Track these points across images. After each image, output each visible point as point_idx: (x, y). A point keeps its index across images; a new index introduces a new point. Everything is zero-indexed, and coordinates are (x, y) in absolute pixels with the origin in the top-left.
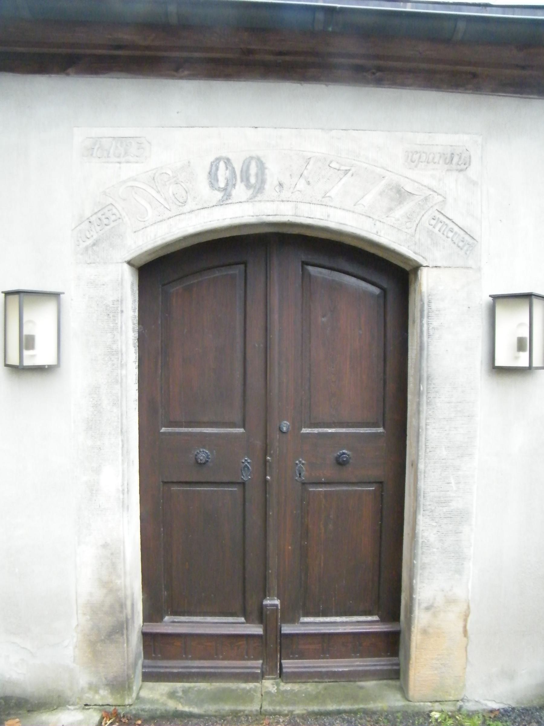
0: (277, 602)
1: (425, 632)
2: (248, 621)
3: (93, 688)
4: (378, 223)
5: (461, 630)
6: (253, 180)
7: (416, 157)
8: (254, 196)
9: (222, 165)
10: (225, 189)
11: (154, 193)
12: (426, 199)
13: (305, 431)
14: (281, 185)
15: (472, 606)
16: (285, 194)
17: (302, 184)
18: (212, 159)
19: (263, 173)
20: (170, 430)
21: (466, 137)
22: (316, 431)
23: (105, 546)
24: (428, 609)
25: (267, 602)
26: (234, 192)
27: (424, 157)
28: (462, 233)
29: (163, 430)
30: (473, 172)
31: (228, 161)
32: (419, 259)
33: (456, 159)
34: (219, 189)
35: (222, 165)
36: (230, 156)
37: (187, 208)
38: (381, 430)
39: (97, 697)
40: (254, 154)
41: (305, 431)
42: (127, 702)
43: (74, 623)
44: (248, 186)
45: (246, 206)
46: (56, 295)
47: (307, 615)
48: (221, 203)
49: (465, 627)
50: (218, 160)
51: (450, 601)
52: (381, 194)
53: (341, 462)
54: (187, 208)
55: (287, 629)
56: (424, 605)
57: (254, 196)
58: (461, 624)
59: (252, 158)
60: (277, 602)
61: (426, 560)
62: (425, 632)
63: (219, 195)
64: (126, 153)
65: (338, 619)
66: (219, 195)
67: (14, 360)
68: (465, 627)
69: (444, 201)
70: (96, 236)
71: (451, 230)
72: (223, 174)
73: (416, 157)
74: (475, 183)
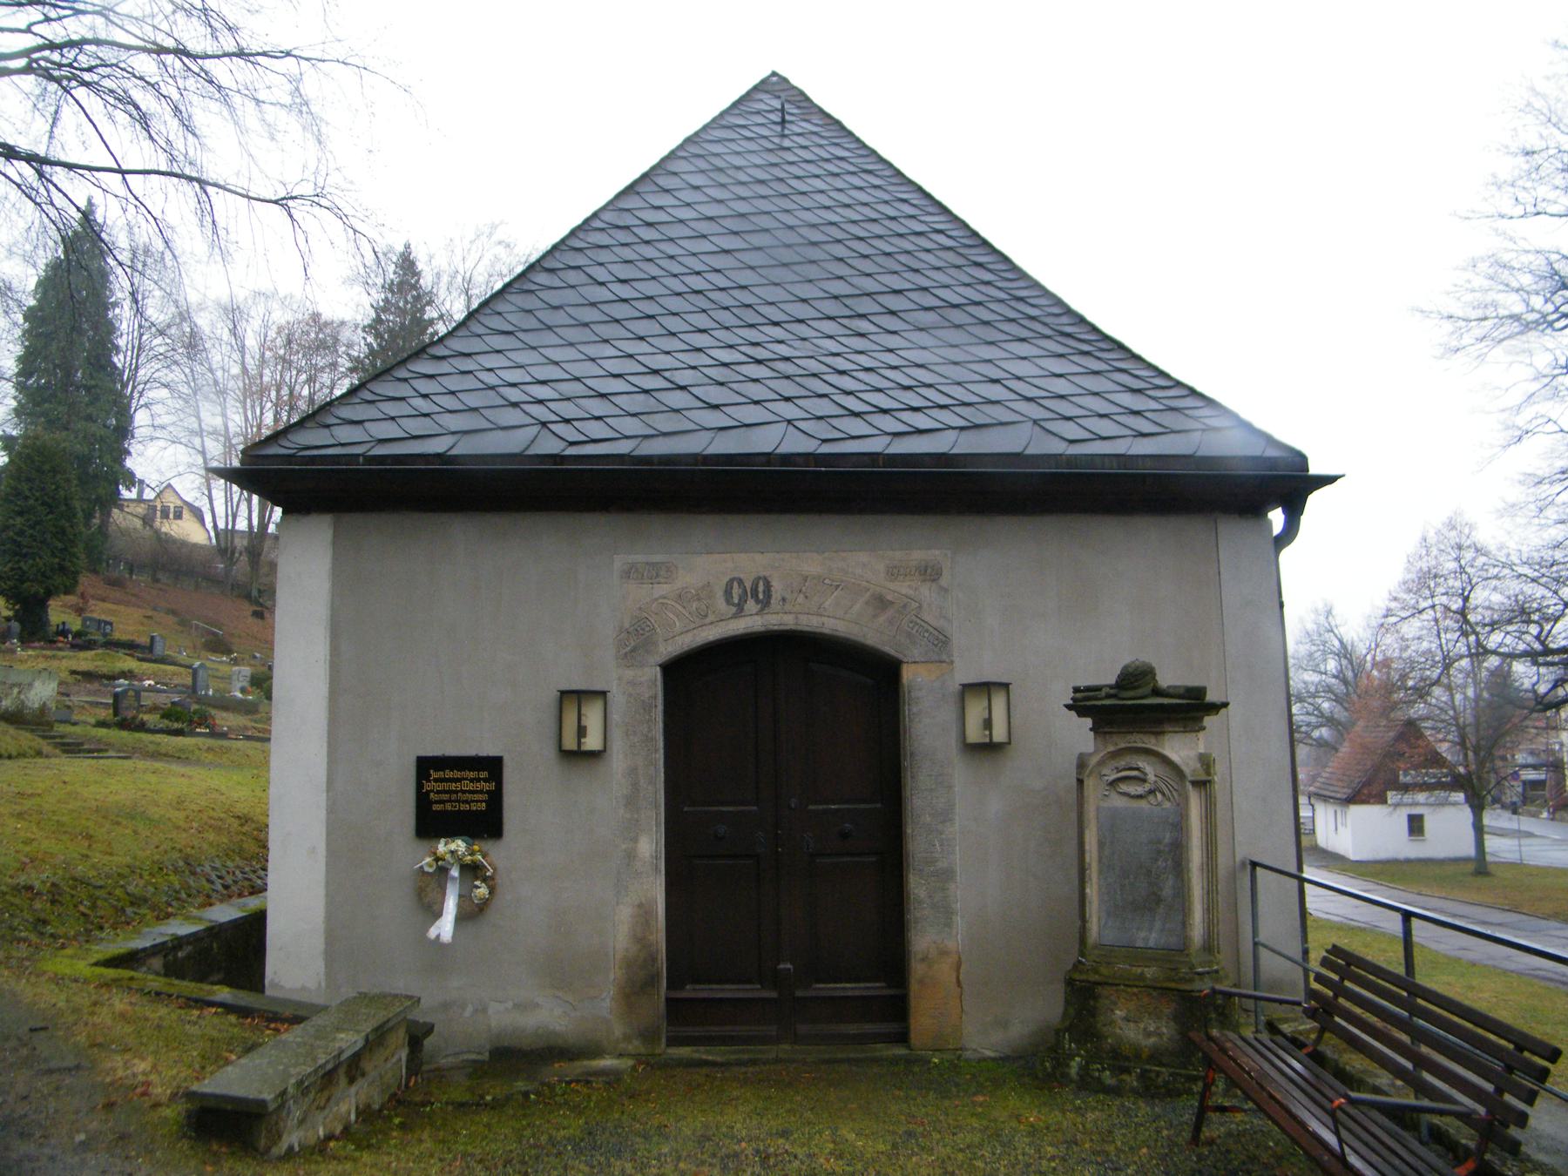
0: (789, 966)
1: (921, 982)
2: (763, 987)
3: (627, 1038)
4: (1474, 582)
5: (954, 980)
6: (761, 596)
7: (895, 571)
8: (762, 609)
9: (735, 584)
10: (739, 604)
11: (680, 608)
12: (905, 606)
13: (811, 807)
14: (784, 600)
15: (963, 958)
16: (788, 607)
17: (801, 599)
18: (727, 579)
19: (769, 590)
20: (691, 809)
21: (937, 552)
22: (821, 807)
23: (640, 906)
24: (923, 960)
25: (781, 966)
26: (746, 607)
27: (902, 571)
28: (936, 633)
29: (686, 809)
30: (944, 581)
31: (740, 582)
32: (900, 656)
33: (929, 571)
34: (733, 605)
35: (735, 584)
36: (742, 576)
37: (708, 620)
38: (879, 805)
39: (630, 1047)
40: (761, 574)
41: (811, 807)
42: (657, 1052)
43: (612, 977)
44: (758, 601)
45: (756, 617)
46: (603, 694)
47: (818, 981)
48: (735, 616)
49: (958, 978)
50: (732, 580)
51: (944, 953)
52: (867, 603)
53: (844, 836)
54: (708, 620)
55: (799, 993)
56: (920, 956)
57: (762, 609)
58: (954, 976)
59: (759, 578)
60: (789, 966)
61: (918, 915)
62: (921, 982)
63: (734, 609)
64: (657, 576)
65: (848, 985)
66: (734, 609)
67: (570, 743)
68: (958, 978)
69: (920, 607)
70: (633, 644)
71: (927, 631)
72: (736, 591)
73: (895, 571)
74: (946, 590)
